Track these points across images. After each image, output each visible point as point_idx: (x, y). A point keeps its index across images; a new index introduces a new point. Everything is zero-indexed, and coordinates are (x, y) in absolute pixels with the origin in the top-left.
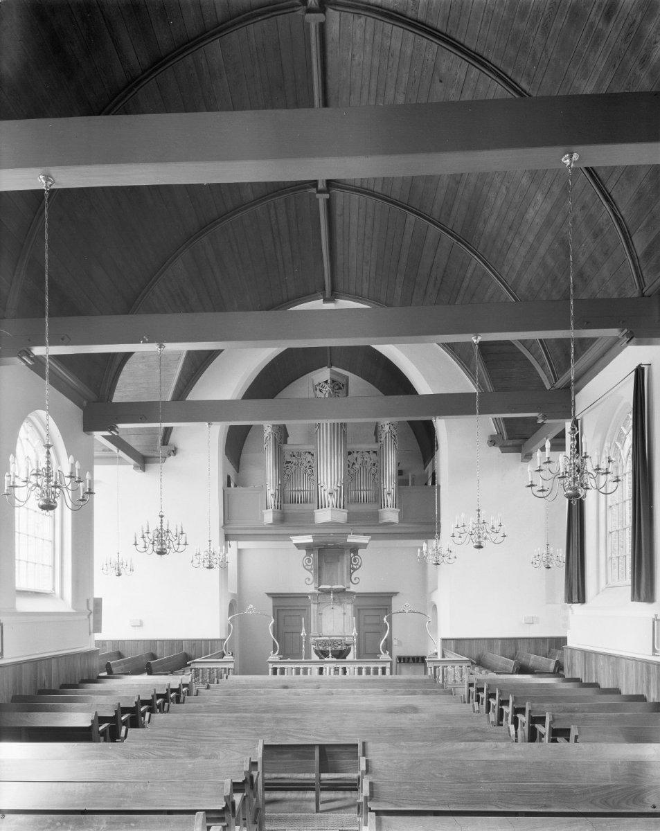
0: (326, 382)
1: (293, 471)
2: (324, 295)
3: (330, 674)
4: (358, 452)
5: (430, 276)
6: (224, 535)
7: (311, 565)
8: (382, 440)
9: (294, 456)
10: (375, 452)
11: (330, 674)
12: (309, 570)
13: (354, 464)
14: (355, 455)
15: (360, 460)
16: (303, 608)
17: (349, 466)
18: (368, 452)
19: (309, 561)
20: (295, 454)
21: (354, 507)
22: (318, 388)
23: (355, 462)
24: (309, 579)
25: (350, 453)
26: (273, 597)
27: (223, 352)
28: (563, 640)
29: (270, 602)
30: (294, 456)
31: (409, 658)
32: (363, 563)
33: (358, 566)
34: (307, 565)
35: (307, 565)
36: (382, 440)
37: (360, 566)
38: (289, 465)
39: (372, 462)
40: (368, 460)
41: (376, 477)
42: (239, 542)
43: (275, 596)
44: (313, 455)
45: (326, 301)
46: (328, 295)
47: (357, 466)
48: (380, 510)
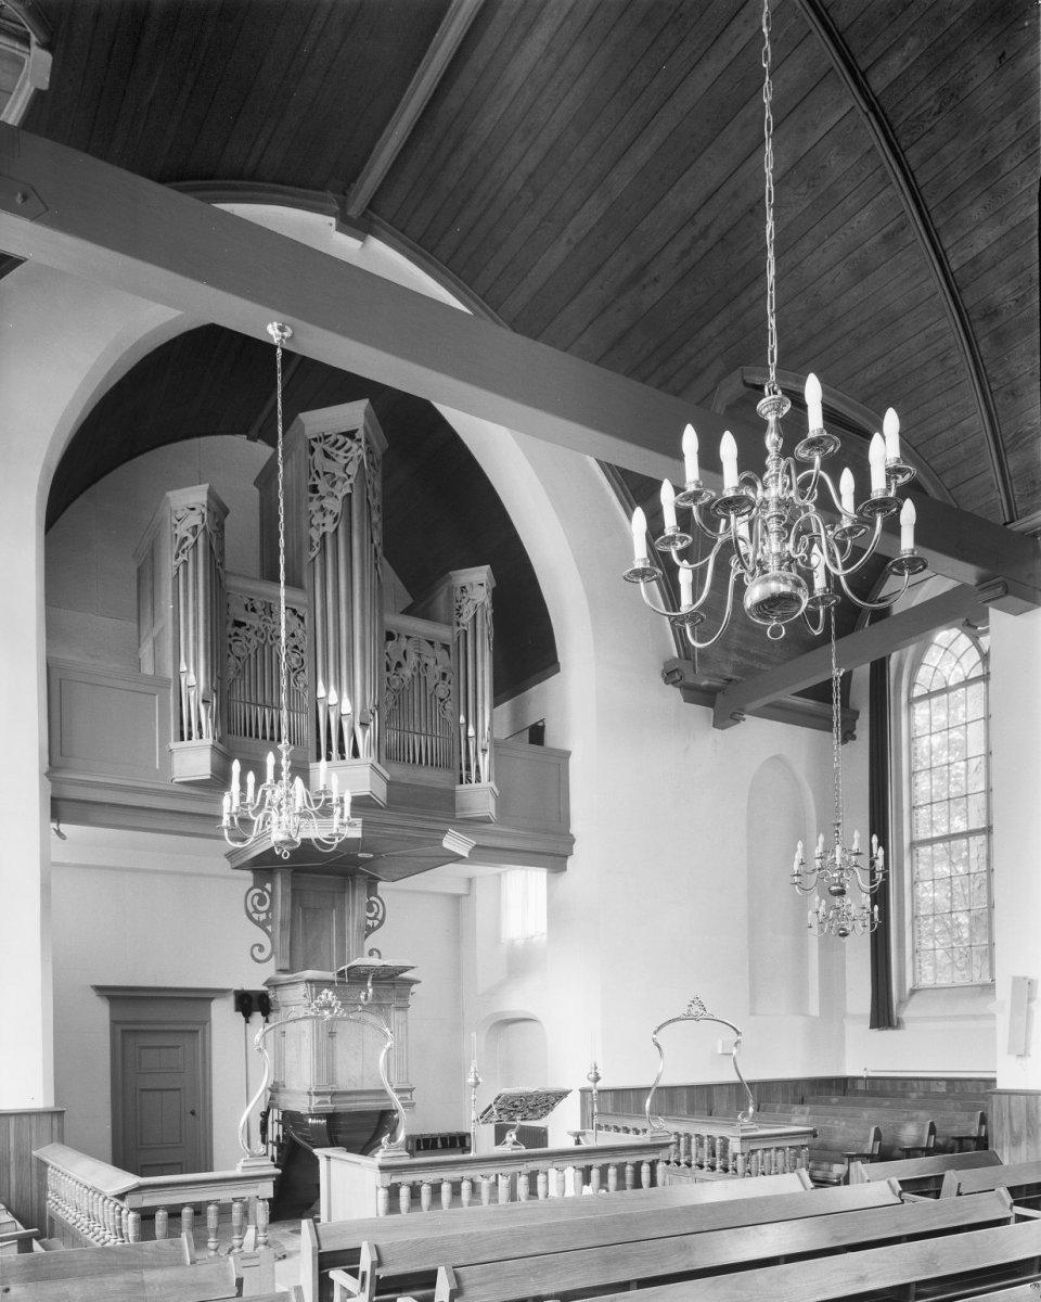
0: (351, 434)
1: (252, 652)
2: (344, 206)
3: (513, 1197)
4: (408, 638)
5: (691, 220)
6: (49, 800)
7: (267, 912)
8: (462, 620)
9: (253, 610)
10: (446, 647)
11: (513, 1197)
12: (262, 925)
13: (399, 665)
14: (404, 643)
15: (413, 658)
16: (190, 1027)
17: (388, 669)
18: (431, 643)
19: (262, 901)
20: (258, 605)
21: (402, 772)
22: (318, 447)
23: (402, 660)
24: (261, 948)
25: (390, 636)
26: (109, 998)
27: (24, 264)
28: (994, 1080)
29: (101, 1011)
30: (253, 610)
31: (435, 1140)
32: (387, 914)
33: (376, 922)
34: (257, 911)
35: (257, 911)
36: (462, 620)
37: (382, 922)
38: (241, 631)
39: (440, 668)
40: (431, 662)
41: (449, 706)
42: (963, 635)
43: (116, 996)
44: (302, 619)
45: (348, 225)
46: (354, 211)
47: (407, 672)
48: (458, 787)
